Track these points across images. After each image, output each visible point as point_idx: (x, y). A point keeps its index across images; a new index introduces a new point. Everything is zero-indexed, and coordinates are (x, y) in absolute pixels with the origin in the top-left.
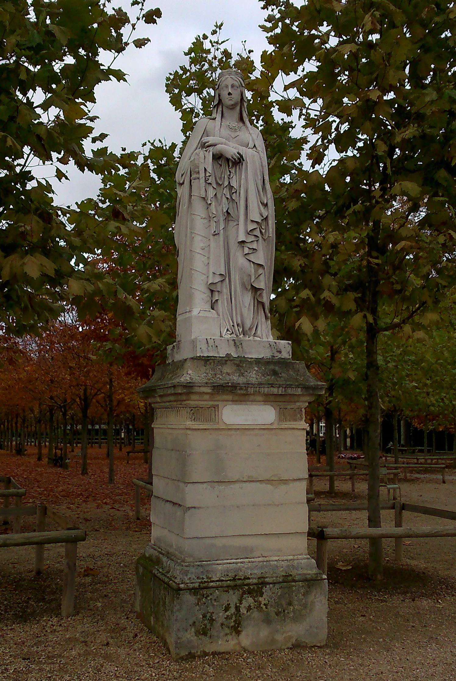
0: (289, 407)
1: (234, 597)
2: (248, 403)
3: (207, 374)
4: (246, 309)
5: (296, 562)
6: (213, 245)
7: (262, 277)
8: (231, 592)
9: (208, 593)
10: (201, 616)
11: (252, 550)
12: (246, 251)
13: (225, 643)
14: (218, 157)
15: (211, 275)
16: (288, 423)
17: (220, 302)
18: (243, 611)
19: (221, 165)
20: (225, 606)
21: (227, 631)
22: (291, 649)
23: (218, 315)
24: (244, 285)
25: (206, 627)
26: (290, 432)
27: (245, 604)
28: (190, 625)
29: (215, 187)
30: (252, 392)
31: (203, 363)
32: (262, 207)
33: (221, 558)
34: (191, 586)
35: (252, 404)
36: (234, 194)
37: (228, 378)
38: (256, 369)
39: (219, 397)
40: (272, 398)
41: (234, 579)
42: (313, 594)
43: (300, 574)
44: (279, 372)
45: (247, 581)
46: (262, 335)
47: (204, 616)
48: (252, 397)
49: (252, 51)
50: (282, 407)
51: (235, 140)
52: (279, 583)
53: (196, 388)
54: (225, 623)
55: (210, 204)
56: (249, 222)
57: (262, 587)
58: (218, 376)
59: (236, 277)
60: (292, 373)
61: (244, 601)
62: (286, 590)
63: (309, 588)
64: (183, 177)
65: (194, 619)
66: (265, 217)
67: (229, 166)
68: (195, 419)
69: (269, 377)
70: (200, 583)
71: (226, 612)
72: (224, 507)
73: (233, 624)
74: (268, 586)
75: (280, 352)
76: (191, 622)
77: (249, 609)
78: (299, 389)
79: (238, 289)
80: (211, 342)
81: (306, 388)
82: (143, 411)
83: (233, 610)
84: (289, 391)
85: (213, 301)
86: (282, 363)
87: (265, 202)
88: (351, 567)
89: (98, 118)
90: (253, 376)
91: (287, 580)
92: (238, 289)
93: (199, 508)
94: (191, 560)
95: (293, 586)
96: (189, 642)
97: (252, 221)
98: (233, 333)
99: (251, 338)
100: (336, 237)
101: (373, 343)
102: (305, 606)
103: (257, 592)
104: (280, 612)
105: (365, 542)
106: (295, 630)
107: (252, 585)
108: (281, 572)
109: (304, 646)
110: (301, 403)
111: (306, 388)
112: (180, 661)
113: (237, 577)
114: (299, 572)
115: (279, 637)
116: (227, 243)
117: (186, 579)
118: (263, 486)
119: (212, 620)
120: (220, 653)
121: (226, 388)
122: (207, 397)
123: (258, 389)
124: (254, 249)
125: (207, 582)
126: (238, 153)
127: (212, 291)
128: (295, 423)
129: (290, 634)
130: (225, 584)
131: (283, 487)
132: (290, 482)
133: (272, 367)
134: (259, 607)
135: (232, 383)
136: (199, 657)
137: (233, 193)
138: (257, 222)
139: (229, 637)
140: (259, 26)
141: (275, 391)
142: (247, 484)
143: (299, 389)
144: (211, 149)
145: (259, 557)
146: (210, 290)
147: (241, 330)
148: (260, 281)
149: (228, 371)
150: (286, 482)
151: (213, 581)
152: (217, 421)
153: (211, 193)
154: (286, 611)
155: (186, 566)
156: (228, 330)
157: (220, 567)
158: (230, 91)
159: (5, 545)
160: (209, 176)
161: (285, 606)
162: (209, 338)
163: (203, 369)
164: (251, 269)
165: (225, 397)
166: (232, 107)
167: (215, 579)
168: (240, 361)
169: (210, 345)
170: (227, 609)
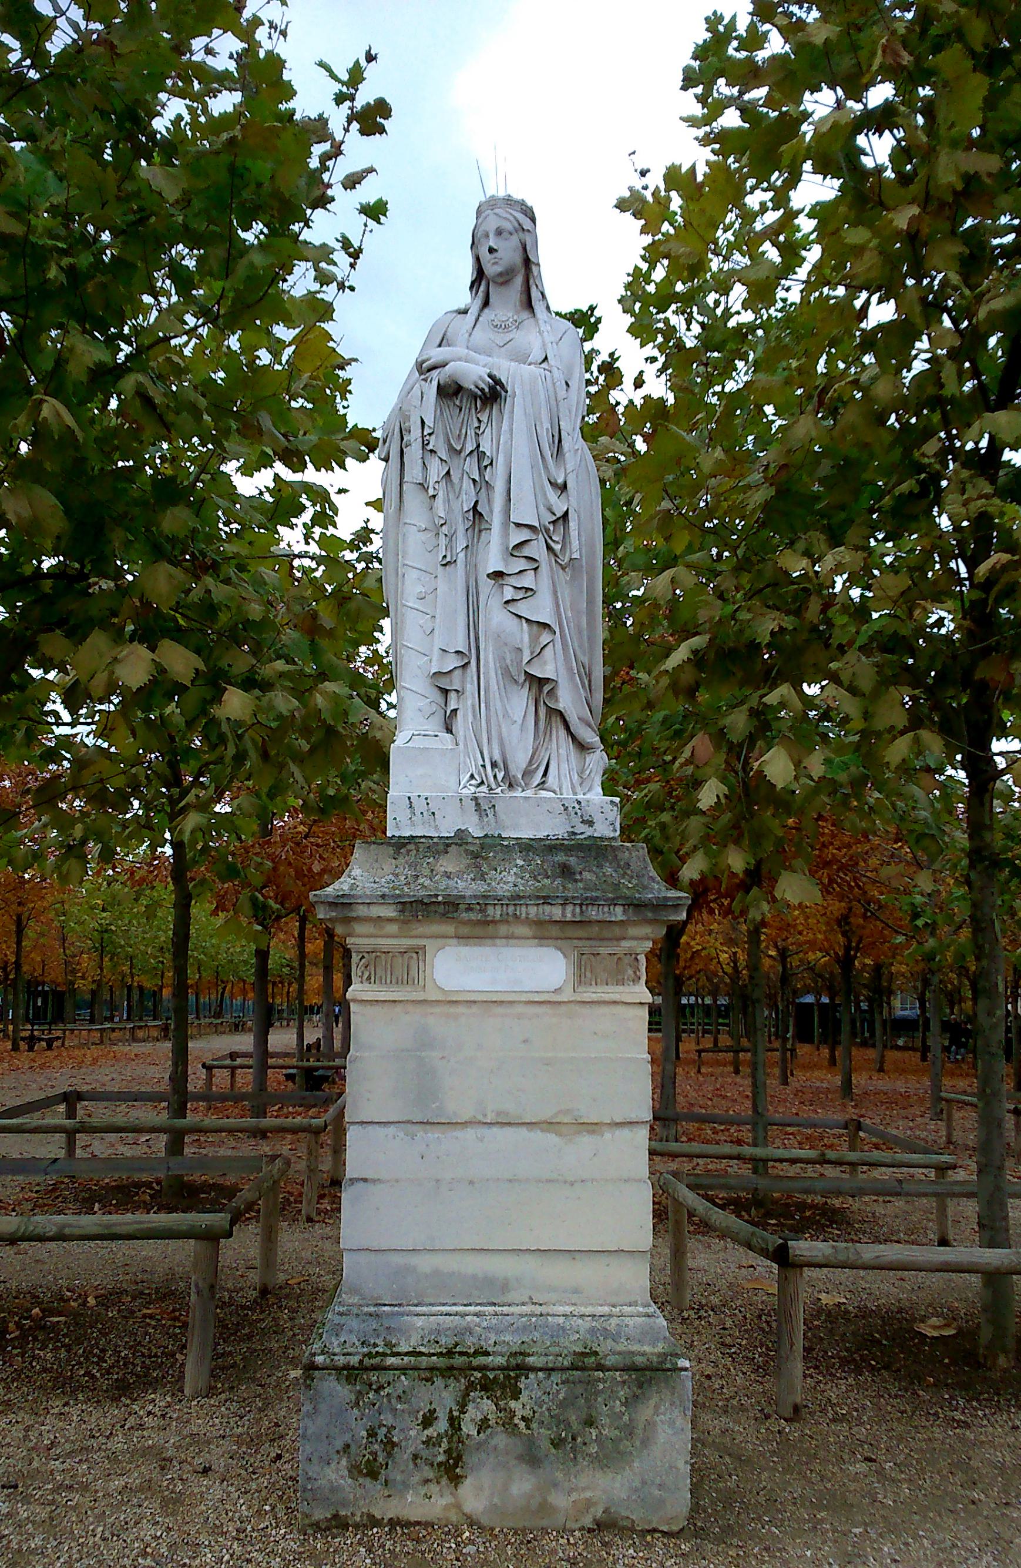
0: (602, 950)
1: (444, 1394)
2: (498, 941)
3: (397, 875)
4: (516, 728)
5: (614, 1321)
6: (442, 587)
7: (548, 652)
8: (439, 1382)
9: (382, 1380)
10: (364, 1433)
11: (505, 1287)
12: (509, 594)
13: (422, 1501)
14: (451, 392)
15: (436, 653)
18: (469, 1428)
20: (424, 1416)
21: (430, 1474)
22: (590, 1531)
24: (506, 673)
25: (375, 1460)
27: (473, 1413)
28: (338, 1452)
30: (498, 917)
31: (391, 850)
32: (552, 495)
33: (427, 1300)
34: (341, 1360)
35: (459, 944)
37: (444, 883)
38: (520, 862)
39: (421, 930)
40: (555, 931)
41: (450, 1353)
42: (652, 1402)
43: (619, 1353)
45: (482, 1360)
47: (372, 1434)
48: (503, 929)
49: (648, 171)
50: (586, 950)
52: (563, 1369)
53: (361, 907)
54: (425, 1453)
55: (434, 496)
57: (517, 1377)
58: (421, 881)
60: (609, 871)
61: (470, 1407)
62: (579, 1389)
63: (640, 1386)
65: (347, 1438)
66: (559, 514)
68: (369, 978)
69: (547, 881)
70: (364, 1356)
71: (425, 1428)
72: (438, 1181)
73: (441, 1458)
74: (532, 1376)
75: (590, 823)
76: (339, 1444)
77: (483, 1425)
78: (619, 910)
79: (493, 682)
80: (420, 806)
81: (637, 906)
82: (729, 970)
83: (442, 1425)
84: (593, 913)
86: (595, 850)
87: (560, 481)
88: (953, 1332)
89: (356, 360)
90: (508, 879)
91: (585, 1364)
92: (493, 682)
93: (374, 1181)
94: (356, 1300)
95: (599, 1380)
96: (334, 1489)
97: (518, 525)
98: (482, 783)
99: (529, 793)
100: (839, 558)
101: (982, 804)
102: (629, 1431)
103: (503, 1387)
104: (563, 1441)
105: (975, 1279)
106: (602, 1488)
107: (493, 1369)
108: (572, 1344)
109: (623, 1528)
110: (634, 943)
111: (637, 906)
112: (310, 1531)
113: (458, 1349)
114: (620, 1348)
115: (561, 1501)
117: (336, 1344)
118: (537, 1135)
119: (390, 1445)
120: (408, 1524)
121: (432, 908)
122: (393, 928)
123: (511, 909)
124: (527, 589)
125: (384, 1355)
126: (490, 376)
127: (445, 692)
128: (621, 988)
129: (588, 1494)
130: (424, 1361)
131: (586, 1141)
132: (604, 1128)
133: (561, 858)
134: (508, 1423)
135: (444, 896)
136: (356, 1526)
139: (434, 1488)
140: (682, 119)
141: (557, 913)
142: (495, 1129)
143: (619, 910)
144: (435, 373)
145: (523, 1304)
148: (545, 663)
149: (449, 869)
150: (590, 1128)
151: (398, 1354)
152: (421, 983)
153: (436, 469)
154: (579, 1440)
155: (341, 1314)
156: (472, 777)
157: (420, 1322)
158: (492, 244)
159: (12, 1240)
161: (575, 1426)
162: (414, 795)
163: (389, 865)
164: (523, 635)
165: (435, 928)
166: (505, 278)
167: (404, 1348)
169: (418, 813)
170: (428, 1421)
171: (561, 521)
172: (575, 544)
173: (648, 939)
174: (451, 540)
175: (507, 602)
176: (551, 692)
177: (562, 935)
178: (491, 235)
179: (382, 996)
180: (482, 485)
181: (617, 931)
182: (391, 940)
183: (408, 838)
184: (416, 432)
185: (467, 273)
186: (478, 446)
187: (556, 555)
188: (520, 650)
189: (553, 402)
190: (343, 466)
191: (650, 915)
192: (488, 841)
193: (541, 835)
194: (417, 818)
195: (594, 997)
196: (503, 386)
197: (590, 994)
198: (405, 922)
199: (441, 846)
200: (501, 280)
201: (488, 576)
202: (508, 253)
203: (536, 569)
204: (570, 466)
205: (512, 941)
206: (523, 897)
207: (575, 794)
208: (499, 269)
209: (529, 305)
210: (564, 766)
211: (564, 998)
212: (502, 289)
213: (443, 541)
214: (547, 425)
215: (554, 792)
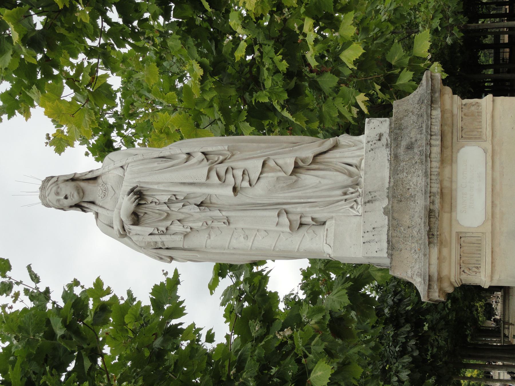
2: (454, 187)
4: (324, 181)
6: (241, 225)
7: (280, 162)
12: (246, 184)
14: (136, 218)
16: (484, 125)
17: (315, 216)
19: (146, 213)
23: (332, 218)
24: (291, 186)
26: (497, 122)
29: (170, 222)
32: (193, 161)
36: (177, 197)
40: (447, 152)
44: (408, 140)
46: (359, 156)
48: (446, 184)
50: (460, 134)
51: (117, 192)
55: (191, 228)
56: (208, 181)
59: (281, 197)
64: (163, 257)
66: (203, 156)
67: (145, 204)
68: (477, 268)
78: (434, 113)
80: (368, 237)
84: (436, 128)
85: (314, 223)
86: (396, 133)
87: (185, 156)
90: (416, 181)
97: (208, 177)
98: (355, 201)
99: (362, 173)
116: (239, 205)
126: (129, 194)
127: (301, 225)
128: (484, 113)
137: (176, 199)
138: (209, 171)
141: (436, 150)
143: (434, 113)
144: (126, 227)
146: (299, 228)
147: (351, 190)
148: (286, 164)
152: (480, 235)
153: (177, 227)
156: (352, 207)
158: (63, 197)
160: (158, 230)
162: (362, 240)
164: (269, 176)
166: (81, 192)
168: (394, 197)
169: (373, 238)
171: (207, 156)
172: (220, 148)
173: (452, 98)
174: (216, 219)
175: (250, 185)
176: (303, 161)
177: (450, 149)
178: (58, 197)
179: (489, 259)
180: (186, 201)
181: (448, 115)
182: (452, 253)
183: (388, 244)
184: (157, 238)
185: (77, 213)
186: (165, 203)
187: (226, 159)
188: (278, 178)
189: (145, 161)
190: (182, 302)
191: (437, 95)
192: (390, 195)
193: (387, 164)
194: (376, 238)
195: (489, 129)
196: (134, 188)
197: (487, 131)
198: (441, 243)
199: (394, 225)
200: (82, 194)
201: (235, 195)
202: (68, 189)
203: (233, 169)
204: (178, 151)
205: (454, 178)
206: (426, 169)
207: (363, 148)
208: (76, 195)
209: (95, 179)
210: (346, 154)
211: (489, 147)
212: (87, 193)
213: (216, 224)
214: (156, 165)
215: (362, 160)
